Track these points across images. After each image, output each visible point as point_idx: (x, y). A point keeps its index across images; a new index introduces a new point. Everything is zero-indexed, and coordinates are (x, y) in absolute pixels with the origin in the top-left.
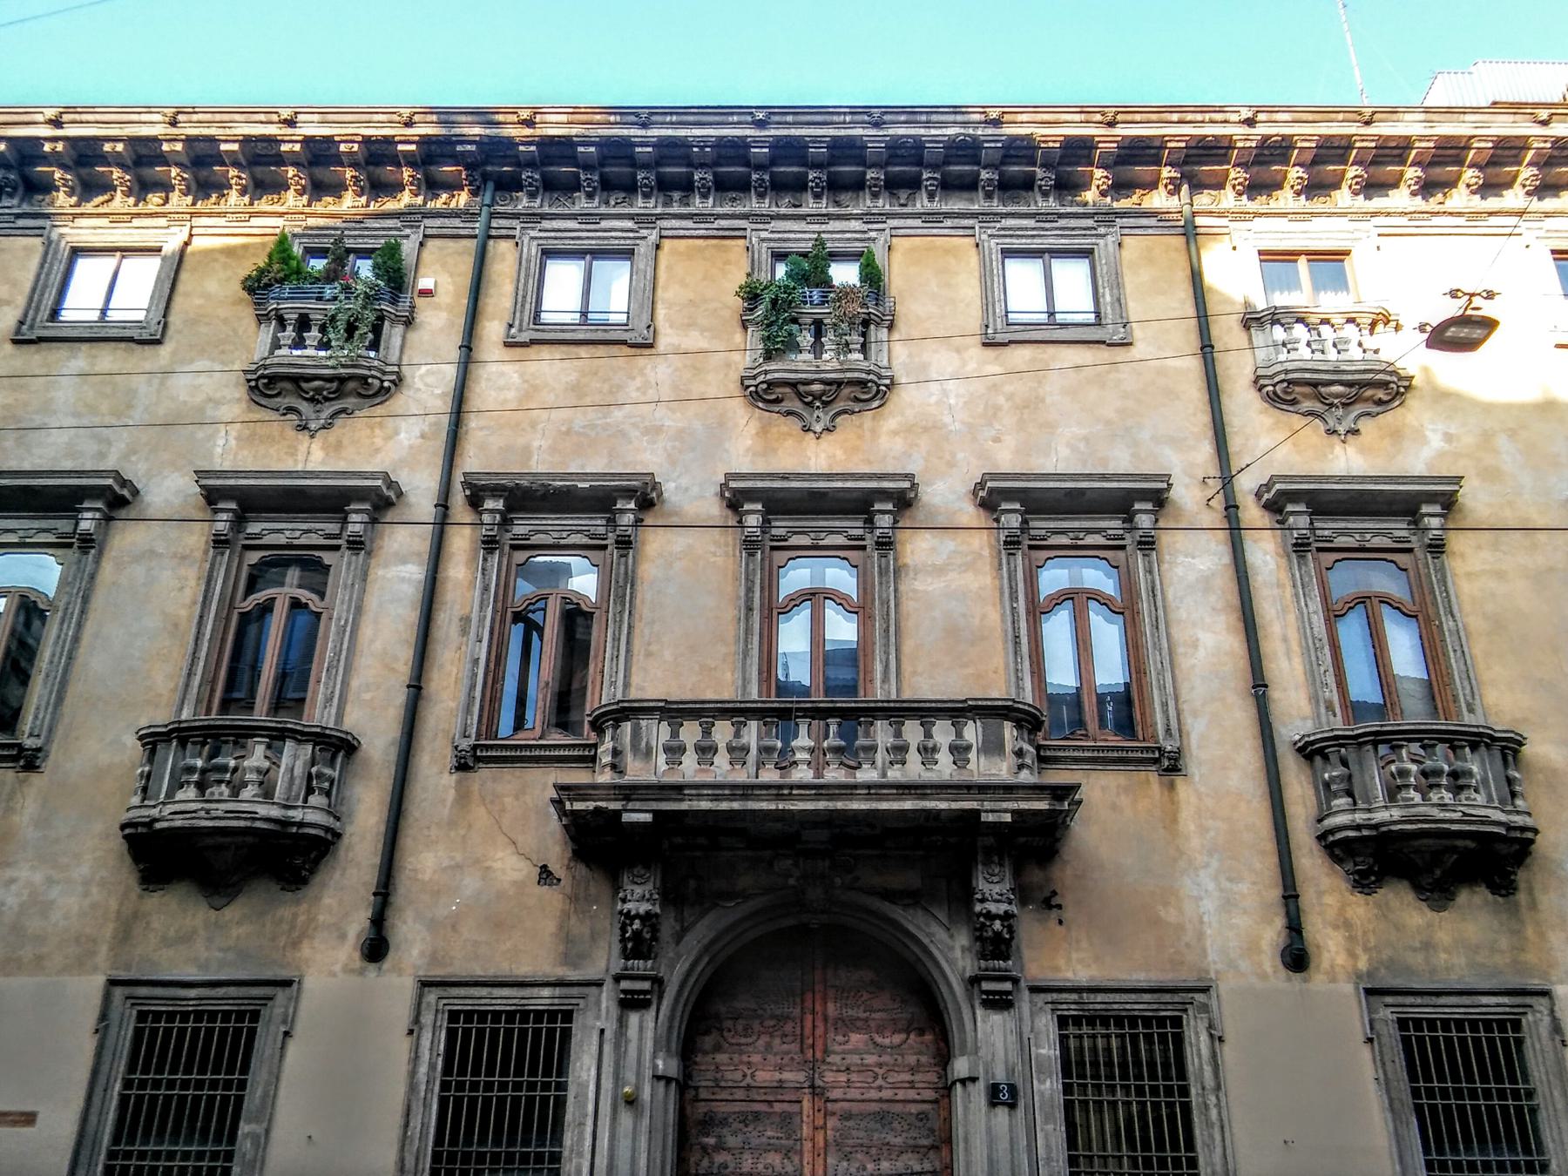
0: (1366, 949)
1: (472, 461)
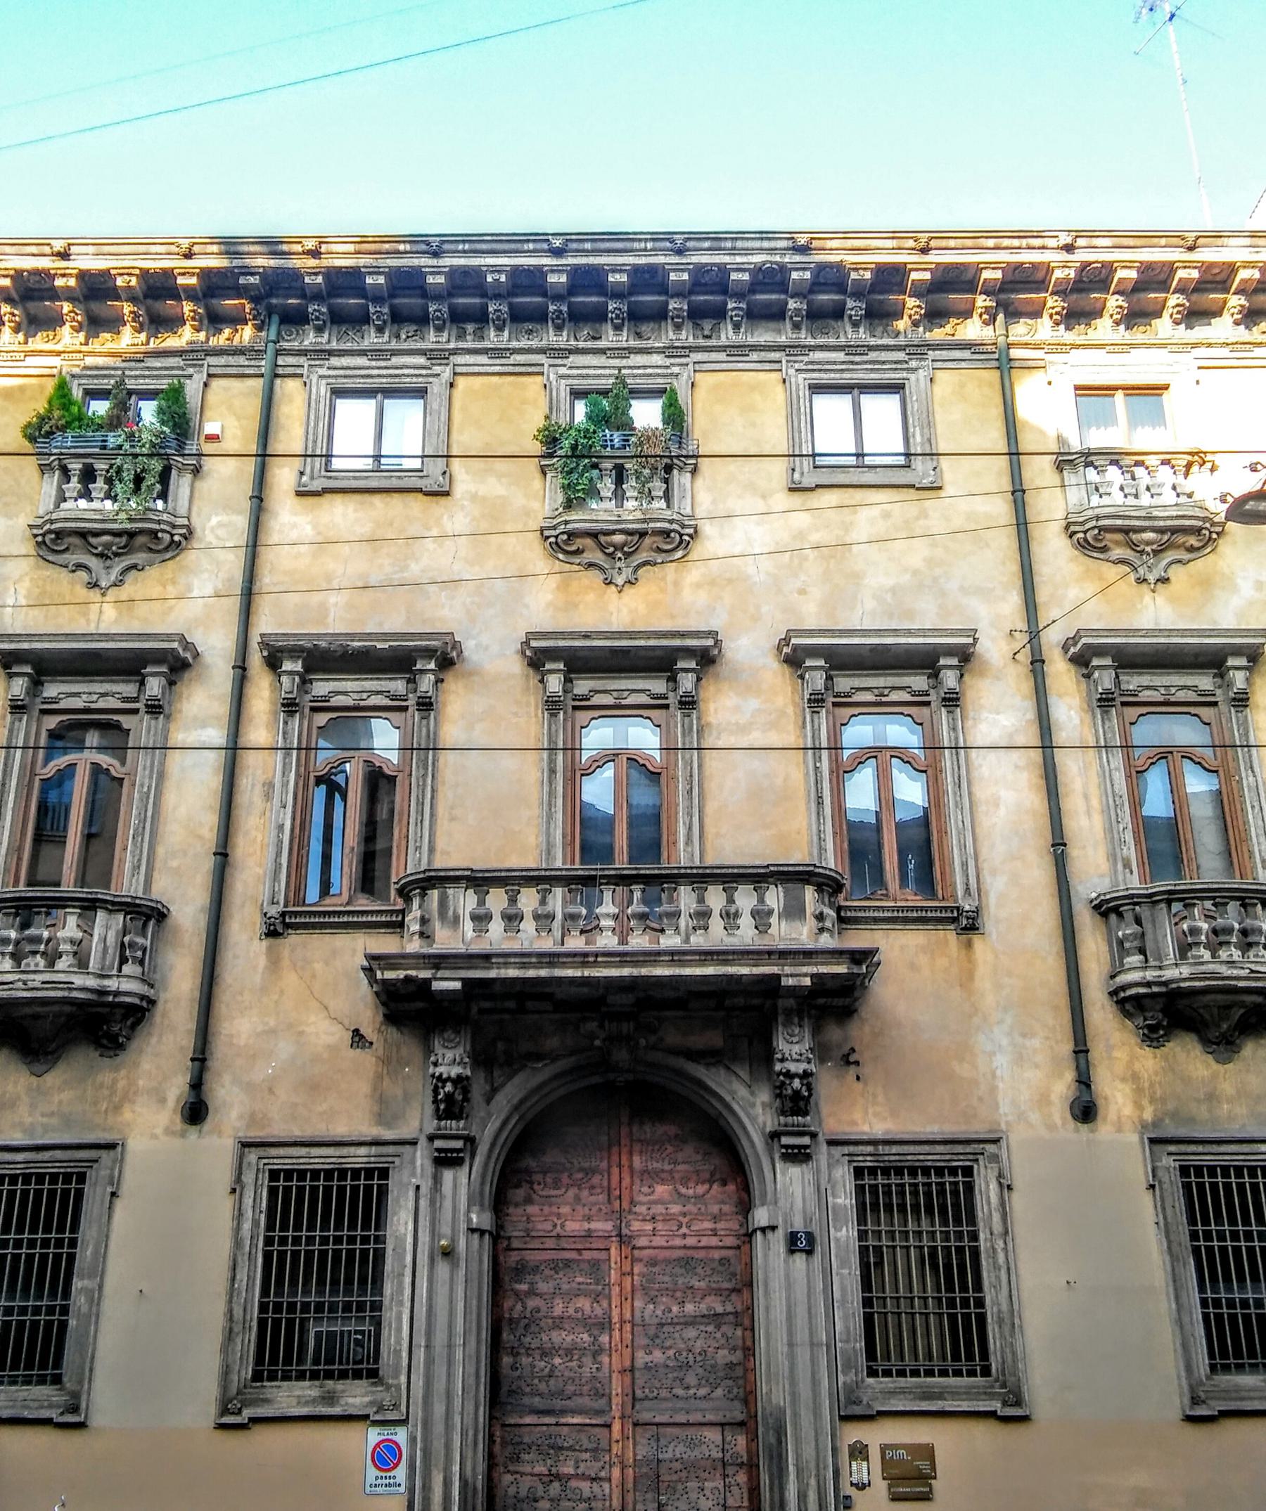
0: (1152, 1100)
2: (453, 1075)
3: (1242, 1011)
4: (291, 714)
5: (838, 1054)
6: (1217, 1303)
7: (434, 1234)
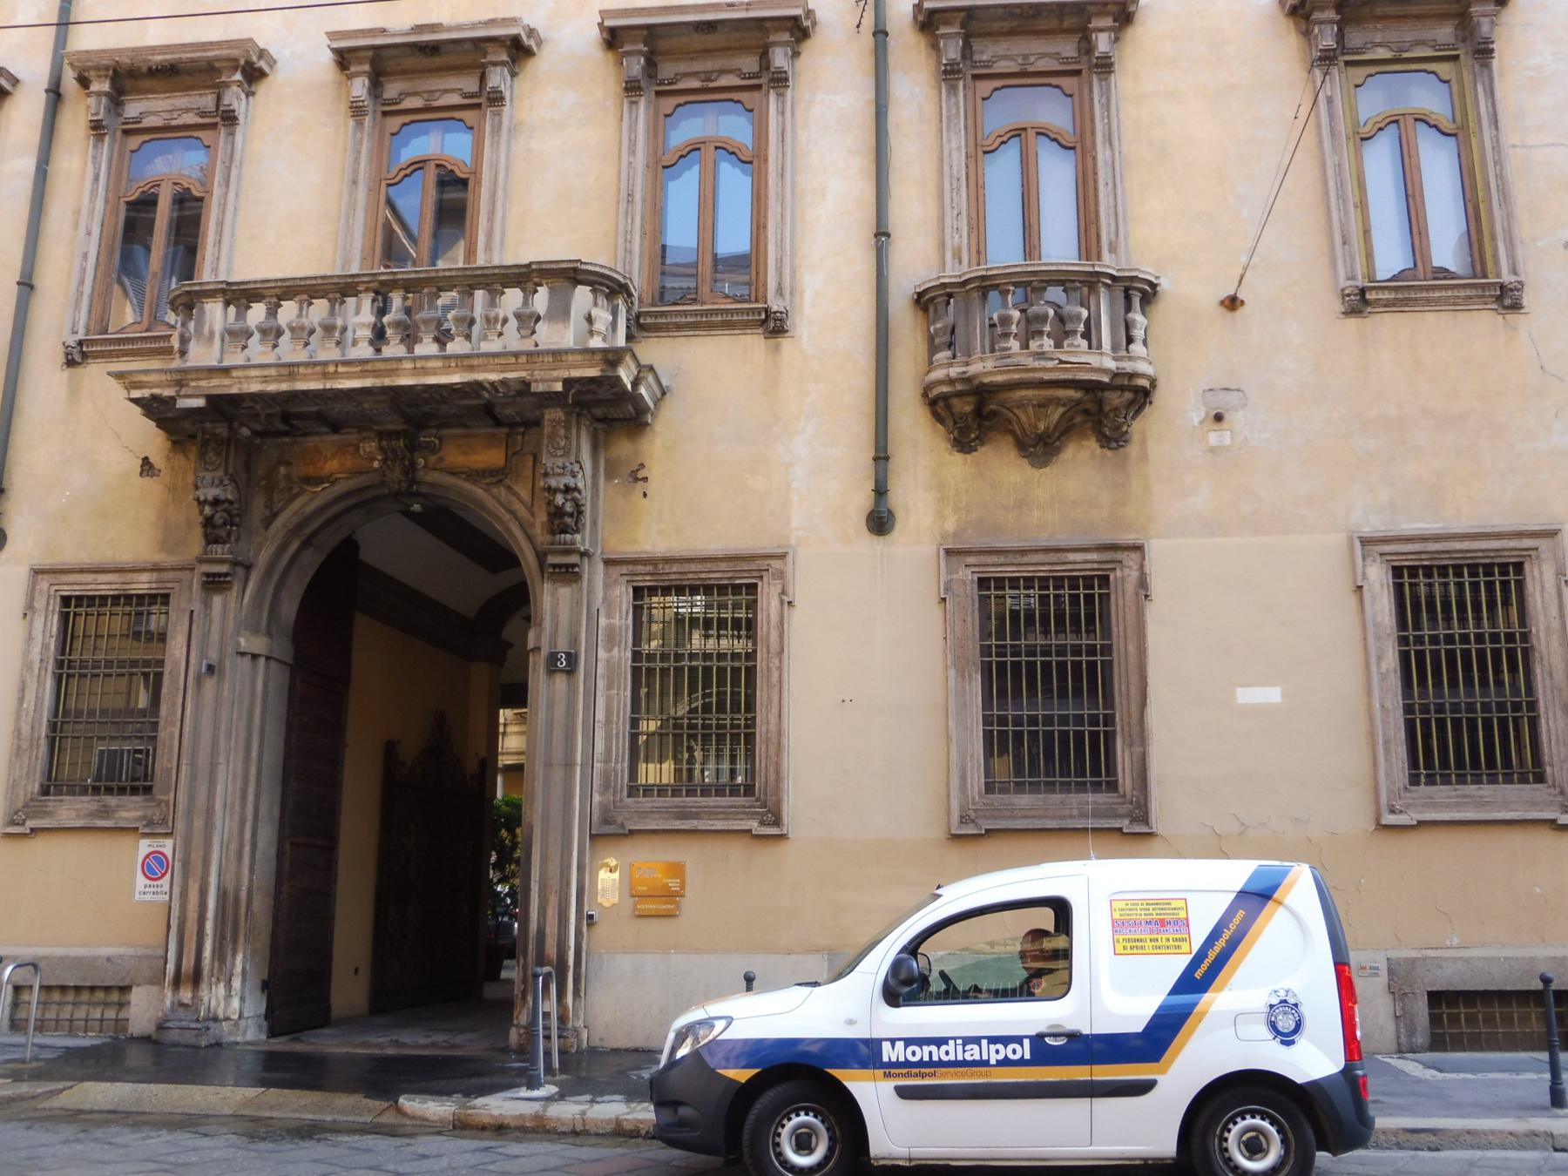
0: (956, 510)
1: (86, 40)
2: (210, 498)
3: (1061, 410)
4: (99, 138)
5: (627, 470)
6: (1002, 721)
7: (203, 655)
